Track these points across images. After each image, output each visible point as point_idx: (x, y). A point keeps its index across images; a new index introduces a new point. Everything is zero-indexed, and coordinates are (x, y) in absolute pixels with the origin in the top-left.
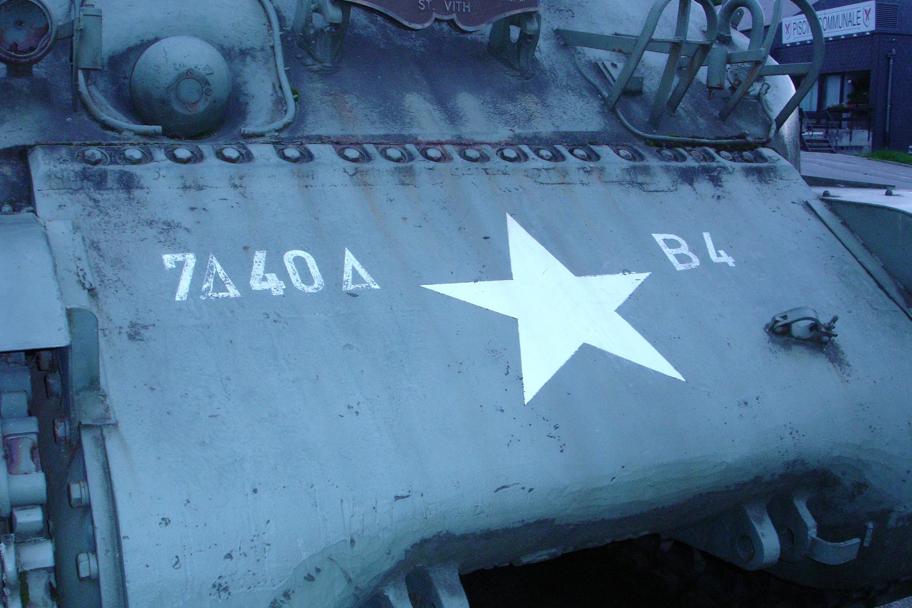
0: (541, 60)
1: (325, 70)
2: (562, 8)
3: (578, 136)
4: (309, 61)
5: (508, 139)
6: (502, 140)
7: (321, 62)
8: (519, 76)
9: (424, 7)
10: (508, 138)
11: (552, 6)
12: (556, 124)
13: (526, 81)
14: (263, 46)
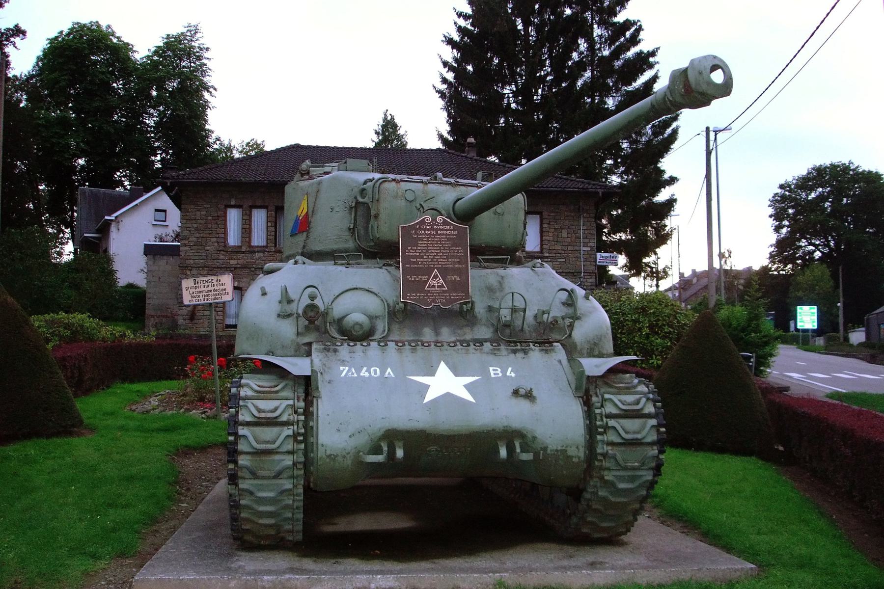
4: (395, 319)
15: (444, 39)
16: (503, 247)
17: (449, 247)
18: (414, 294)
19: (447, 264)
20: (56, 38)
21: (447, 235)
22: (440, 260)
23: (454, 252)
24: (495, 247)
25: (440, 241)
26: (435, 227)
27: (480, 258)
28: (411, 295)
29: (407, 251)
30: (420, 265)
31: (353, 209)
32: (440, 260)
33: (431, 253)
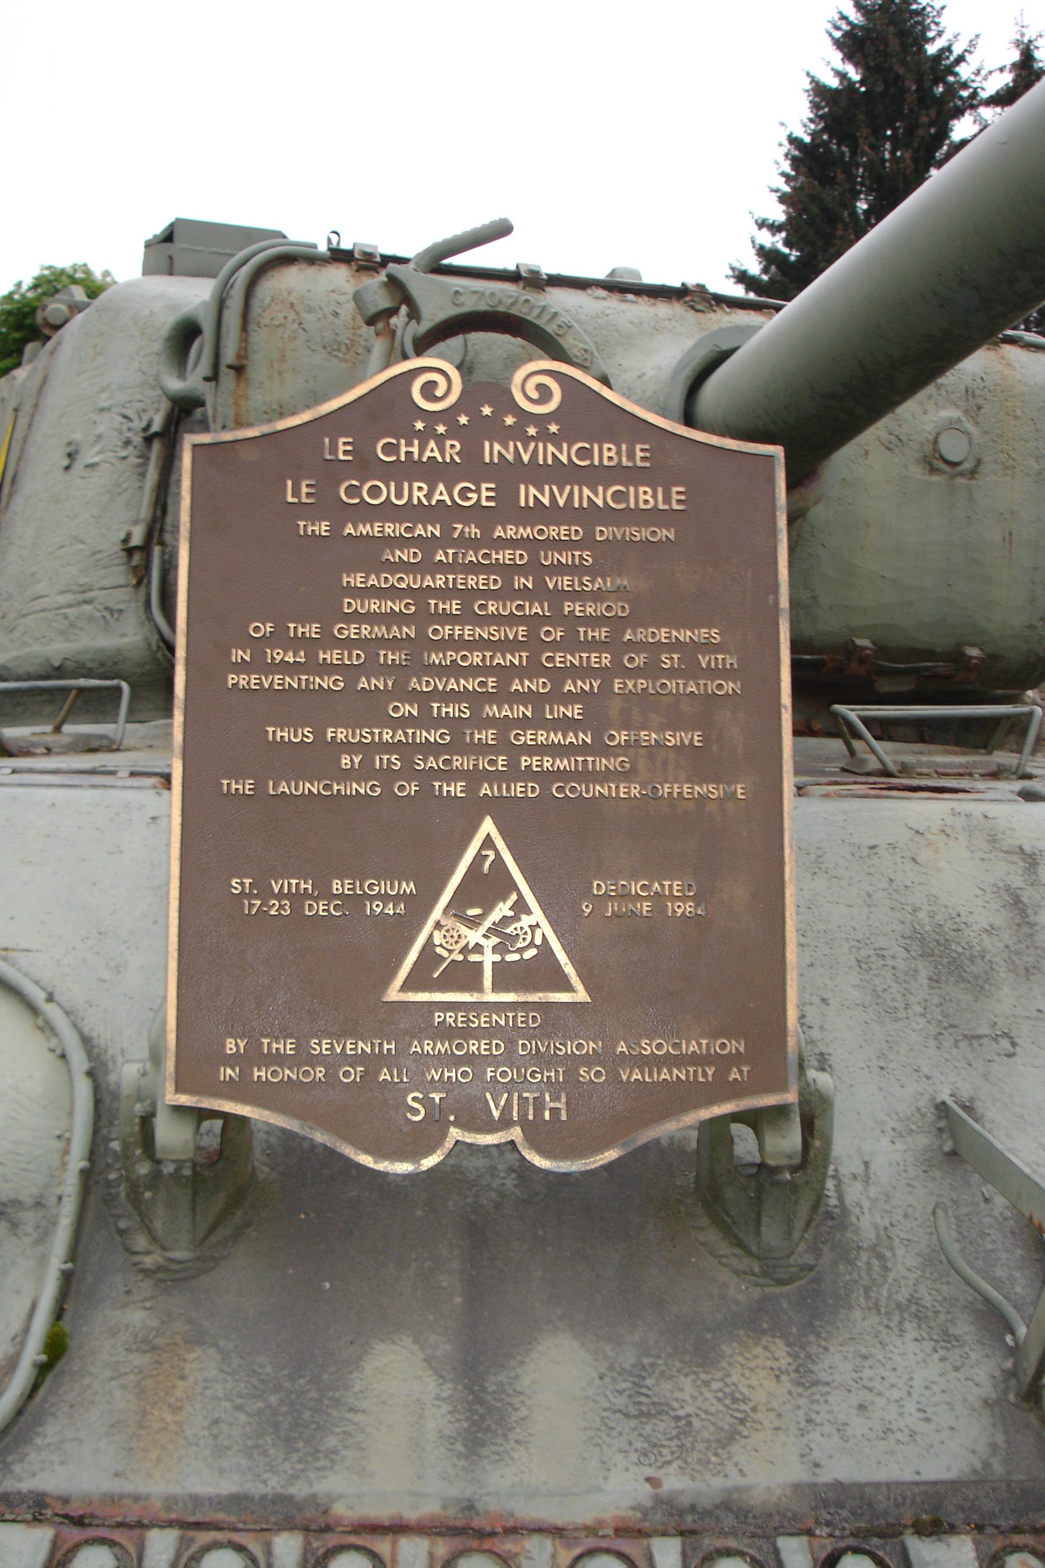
0: (857, 1210)
1: (171, 1271)
2: (980, 1031)
3: (881, 1497)
4: (141, 1242)
5: (631, 1513)
6: (608, 1516)
7: (163, 1248)
8: (755, 1275)
9: (423, 1112)
10: (633, 1508)
11: (951, 1026)
12: (816, 1455)
13: (778, 1290)
14: (42, 1196)
15: (730, 273)
16: (973, 652)
17: (617, 624)
18: (288, 1047)
19: (586, 776)
20: (11, 294)
21: (592, 515)
22: (528, 737)
23: (652, 671)
24: (930, 654)
25: (534, 568)
26: (492, 450)
27: (852, 713)
28: (253, 1057)
29: (238, 655)
30: (347, 775)
31: (157, 446)
32: (528, 737)
33: (454, 670)
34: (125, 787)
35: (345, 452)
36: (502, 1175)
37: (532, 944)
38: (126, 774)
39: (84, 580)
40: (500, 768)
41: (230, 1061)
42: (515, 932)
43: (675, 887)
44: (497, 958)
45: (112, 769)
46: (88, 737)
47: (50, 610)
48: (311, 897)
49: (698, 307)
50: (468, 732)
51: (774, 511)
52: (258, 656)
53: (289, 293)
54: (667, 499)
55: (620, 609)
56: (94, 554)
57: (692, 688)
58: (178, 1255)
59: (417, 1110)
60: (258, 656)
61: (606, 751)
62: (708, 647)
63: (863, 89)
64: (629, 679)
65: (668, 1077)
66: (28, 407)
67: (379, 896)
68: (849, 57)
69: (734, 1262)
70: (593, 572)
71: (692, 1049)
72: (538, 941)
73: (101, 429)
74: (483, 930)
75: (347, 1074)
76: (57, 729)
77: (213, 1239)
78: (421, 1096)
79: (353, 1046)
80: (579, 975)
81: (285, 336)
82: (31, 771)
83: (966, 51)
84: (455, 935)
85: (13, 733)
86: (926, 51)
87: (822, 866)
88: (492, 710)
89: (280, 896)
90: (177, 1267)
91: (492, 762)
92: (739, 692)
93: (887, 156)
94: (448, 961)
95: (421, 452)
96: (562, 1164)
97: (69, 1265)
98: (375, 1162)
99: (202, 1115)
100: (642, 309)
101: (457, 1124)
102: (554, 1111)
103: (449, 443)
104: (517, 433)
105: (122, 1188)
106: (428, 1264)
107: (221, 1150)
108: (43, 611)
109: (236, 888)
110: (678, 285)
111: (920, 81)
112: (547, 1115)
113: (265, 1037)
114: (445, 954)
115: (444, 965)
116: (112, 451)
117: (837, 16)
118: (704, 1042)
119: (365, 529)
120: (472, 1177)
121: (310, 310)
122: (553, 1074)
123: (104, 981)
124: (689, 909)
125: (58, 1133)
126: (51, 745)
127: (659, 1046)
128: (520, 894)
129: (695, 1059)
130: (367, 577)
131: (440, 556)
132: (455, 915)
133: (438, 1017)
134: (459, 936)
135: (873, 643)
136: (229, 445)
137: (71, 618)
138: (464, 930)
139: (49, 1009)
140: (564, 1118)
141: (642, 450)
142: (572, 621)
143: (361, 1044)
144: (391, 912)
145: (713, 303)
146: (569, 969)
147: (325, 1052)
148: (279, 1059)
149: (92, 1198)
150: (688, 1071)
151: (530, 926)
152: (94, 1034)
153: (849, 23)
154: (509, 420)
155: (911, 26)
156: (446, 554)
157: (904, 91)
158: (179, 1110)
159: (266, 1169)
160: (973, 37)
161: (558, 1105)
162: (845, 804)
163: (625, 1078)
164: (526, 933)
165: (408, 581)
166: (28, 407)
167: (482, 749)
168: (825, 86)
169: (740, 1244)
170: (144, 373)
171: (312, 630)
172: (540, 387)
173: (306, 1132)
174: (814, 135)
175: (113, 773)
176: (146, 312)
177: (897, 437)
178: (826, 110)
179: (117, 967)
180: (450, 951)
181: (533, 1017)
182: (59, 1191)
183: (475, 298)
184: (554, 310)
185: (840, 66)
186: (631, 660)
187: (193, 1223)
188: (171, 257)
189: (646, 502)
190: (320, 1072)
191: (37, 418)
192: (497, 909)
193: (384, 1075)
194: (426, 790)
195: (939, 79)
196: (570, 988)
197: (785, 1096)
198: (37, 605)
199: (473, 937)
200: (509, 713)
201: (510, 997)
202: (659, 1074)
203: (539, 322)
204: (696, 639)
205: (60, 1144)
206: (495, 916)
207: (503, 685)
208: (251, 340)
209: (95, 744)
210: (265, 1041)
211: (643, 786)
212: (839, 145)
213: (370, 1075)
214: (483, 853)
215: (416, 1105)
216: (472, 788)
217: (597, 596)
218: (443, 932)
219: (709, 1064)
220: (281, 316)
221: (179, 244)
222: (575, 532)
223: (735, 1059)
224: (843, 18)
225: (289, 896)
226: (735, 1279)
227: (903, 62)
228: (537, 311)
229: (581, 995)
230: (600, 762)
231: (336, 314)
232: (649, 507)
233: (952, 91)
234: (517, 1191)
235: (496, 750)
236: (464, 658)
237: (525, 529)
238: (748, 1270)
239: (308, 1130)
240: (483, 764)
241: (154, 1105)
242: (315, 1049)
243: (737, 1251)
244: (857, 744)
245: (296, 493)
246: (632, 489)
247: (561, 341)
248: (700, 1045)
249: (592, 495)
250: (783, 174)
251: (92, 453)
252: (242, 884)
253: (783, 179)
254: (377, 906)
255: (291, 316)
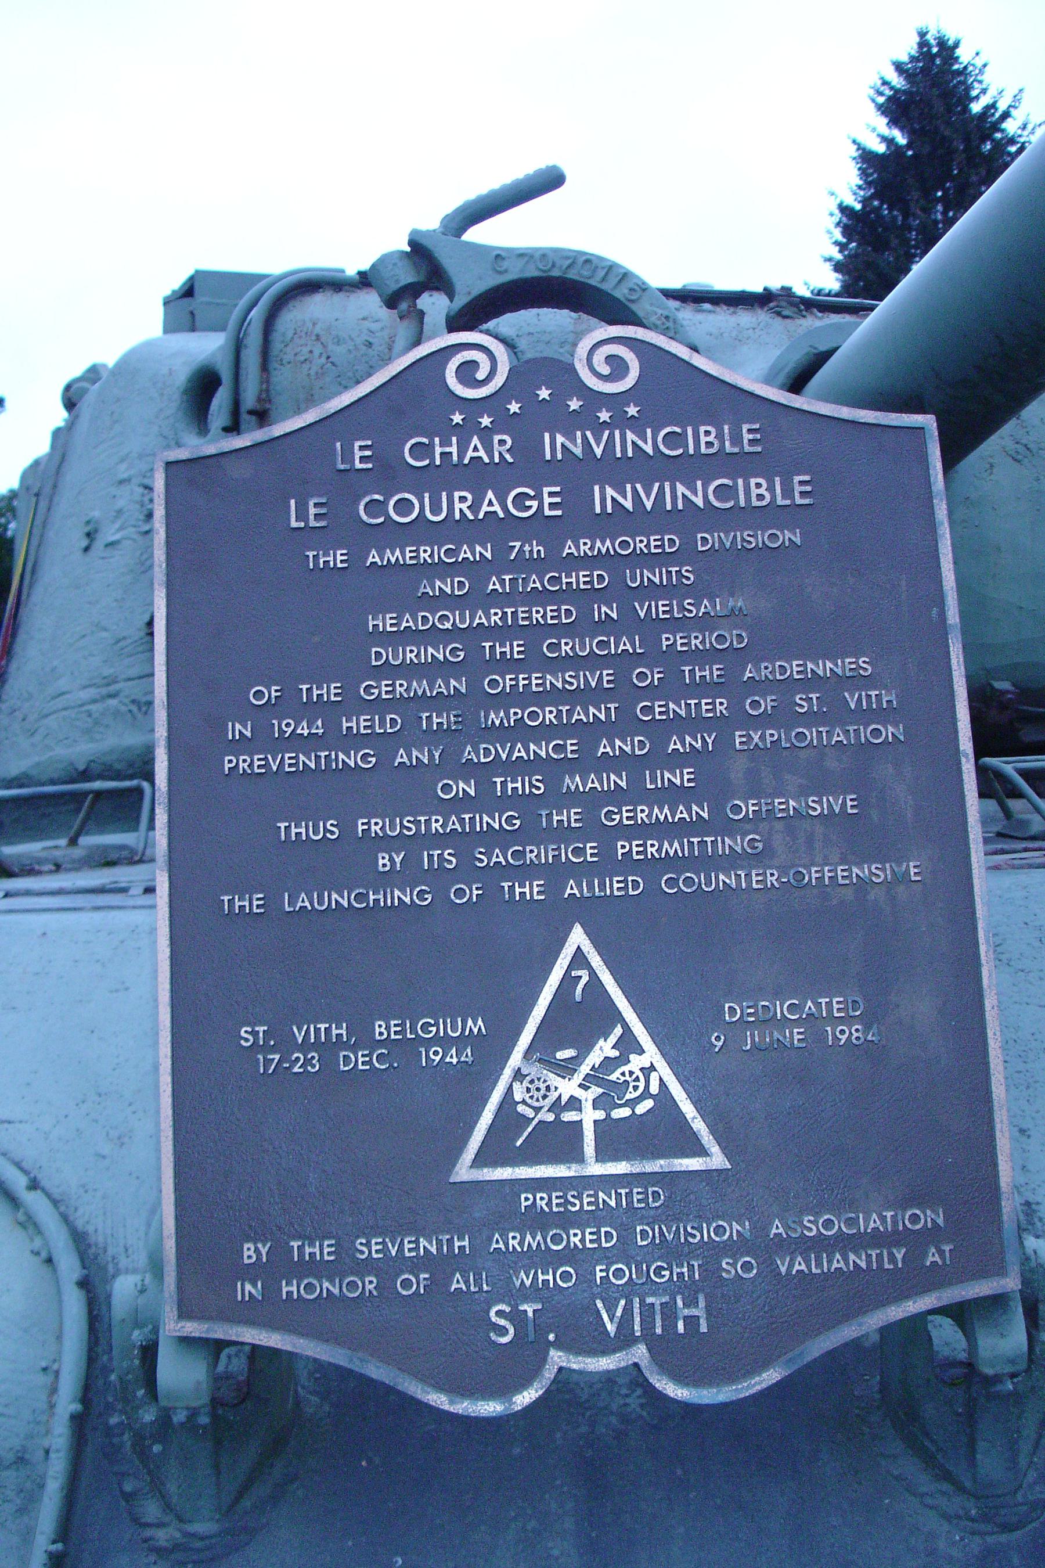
1: (191, 1549)
4: (151, 1510)
7: (181, 1520)
8: (973, 1520)
9: (512, 1331)
13: (1003, 1538)
14: (24, 1449)
17: (735, 658)
18: (325, 1250)
29: (238, 729)
30: (387, 880)
33: (520, 732)
34: (134, 907)
35: (363, 459)
36: (624, 1391)
37: (646, 1094)
38: (141, 890)
39: (107, 671)
40: (589, 859)
41: (251, 1273)
42: (623, 1079)
43: (836, 1006)
44: (600, 1115)
45: (123, 885)
46: (106, 848)
47: (73, 708)
48: (346, 1046)
49: (786, 313)
50: (544, 813)
51: (930, 498)
52: (262, 730)
53: (314, 324)
54: (788, 492)
55: (735, 637)
56: (118, 641)
57: (838, 736)
58: (199, 1527)
59: (504, 1327)
60: (262, 730)
61: (729, 828)
62: (855, 681)
63: (910, 153)
64: (755, 731)
65: (842, 1265)
66: (47, 490)
67: (436, 1040)
68: (894, 121)
69: (942, 1502)
70: (697, 592)
71: (872, 1225)
72: (654, 1089)
73: (121, 503)
74: (578, 1078)
75: (407, 1284)
76: (73, 842)
77: (247, 1503)
78: (508, 1309)
79: (412, 1246)
80: (713, 1132)
81: (312, 372)
82: (28, 893)
83: (1010, 106)
84: (543, 1086)
85: (14, 851)
86: (970, 111)
87: (1003, 957)
88: (573, 782)
89: (305, 1046)
90: (199, 1544)
91: (577, 851)
92: (902, 738)
93: (939, 217)
94: (534, 1123)
95: (462, 453)
96: (705, 1392)
97: (59, 1546)
98: (451, 1402)
99: (218, 1346)
100: (721, 319)
101: (558, 1345)
102: (689, 1320)
103: (496, 438)
104: (585, 420)
105: (126, 1437)
106: (532, 1524)
107: (248, 1383)
108: (65, 709)
109: (247, 1040)
110: (759, 289)
111: (967, 140)
112: (681, 1327)
113: (294, 1238)
114: (530, 1113)
115: (530, 1129)
116: (135, 526)
117: (879, 82)
118: (889, 1214)
119: (393, 556)
120: (584, 1397)
121: (338, 341)
122: (685, 1270)
123: (104, 1157)
124: (856, 1035)
125: (44, 1364)
126: (60, 861)
127: (828, 1224)
128: (627, 1029)
129: (876, 1239)
130: (399, 618)
131: (494, 584)
132: (540, 1060)
133: (525, 1200)
134: (548, 1088)
135: (1014, 685)
136: (214, 460)
137: (96, 715)
138: (554, 1080)
139: (34, 1200)
140: (704, 1328)
141: (750, 431)
142: (673, 658)
143: (423, 1242)
144: (455, 1061)
145: (803, 307)
146: (699, 1125)
147: (375, 1256)
148: (313, 1268)
149: (89, 1451)
150: (869, 1256)
151: (642, 1069)
152: (90, 1229)
153: (892, 88)
154: (574, 404)
155: (955, 87)
156: (502, 582)
157: (951, 152)
158: (186, 1341)
159: (315, 1399)
160: (1017, 92)
161: (694, 1312)
162: (1025, 877)
163: (783, 1270)
164: (637, 1079)
165: (455, 620)
166: (47, 490)
167: (563, 834)
168: (871, 153)
169: (946, 1476)
170: (165, 437)
171: (331, 691)
172: (610, 359)
173: (356, 1366)
174: (865, 202)
175: (124, 890)
176: (165, 371)
177: (1026, 446)
178: (875, 176)
179: (119, 1138)
180: (536, 1110)
181: (654, 1192)
182: (46, 1443)
183: (520, 263)
184: (623, 271)
185: (886, 131)
186: (755, 704)
187: (218, 1484)
188: (192, 313)
189: (761, 497)
190: (371, 1284)
191: (56, 499)
192: (597, 1047)
193: (457, 1283)
194: (491, 894)
195: (986, 137)
196: (703, 1152)
197: (1003, 1282)
198: (60, 703)
199: (567, 1088)
200: (597, 785)
201: (620, 1168)
202: (830, 1262)
203: (606, 287)
204: (839, 671)
205: (47, 1379)
206: (595, 1058)
207: (586, 747)
208: (274, 380)
209: (114, 856)
210: (295, 1244)
211: (783, 870)
212: (890, 209)
213: (438, 1283)
214: (573, 974)
215: (502, 1322)
216: (554, 887)
217: (705, 623)
218: (526, 1084)
219: (898, 1244)
220: (305, 350)
221: (200, 298)
222: (671, 541)
223: (933, 1235)
224: (885, 83)
225: (317, 1046)
226: (946, 1526)
227: (948, 123)
228: (601, 274)
229: (717, 1160)
230: (723, 842)
231: (370, 345)
232: (764, 503)
233: (1000, 147)
234: (645, 1414)
235: (582, 834)
236: (533, 715)
237: (603, 543)
238: (961, 1512)
239: (358, 1363)
240: (567, 854)
241: (156, 1330)
242: (362, 1252)
243: (946, 1486)
244: (1014, 805)
245: (302, 515)
246: (740, 481)
247: (634, 307)
248: (883, 1219)
249: (688, 493)
250: (837, 243)
251: (113, 531)
252: (255, 1033)
253: (837, 248)
254: (436, 1053)
255: (318, 350)
